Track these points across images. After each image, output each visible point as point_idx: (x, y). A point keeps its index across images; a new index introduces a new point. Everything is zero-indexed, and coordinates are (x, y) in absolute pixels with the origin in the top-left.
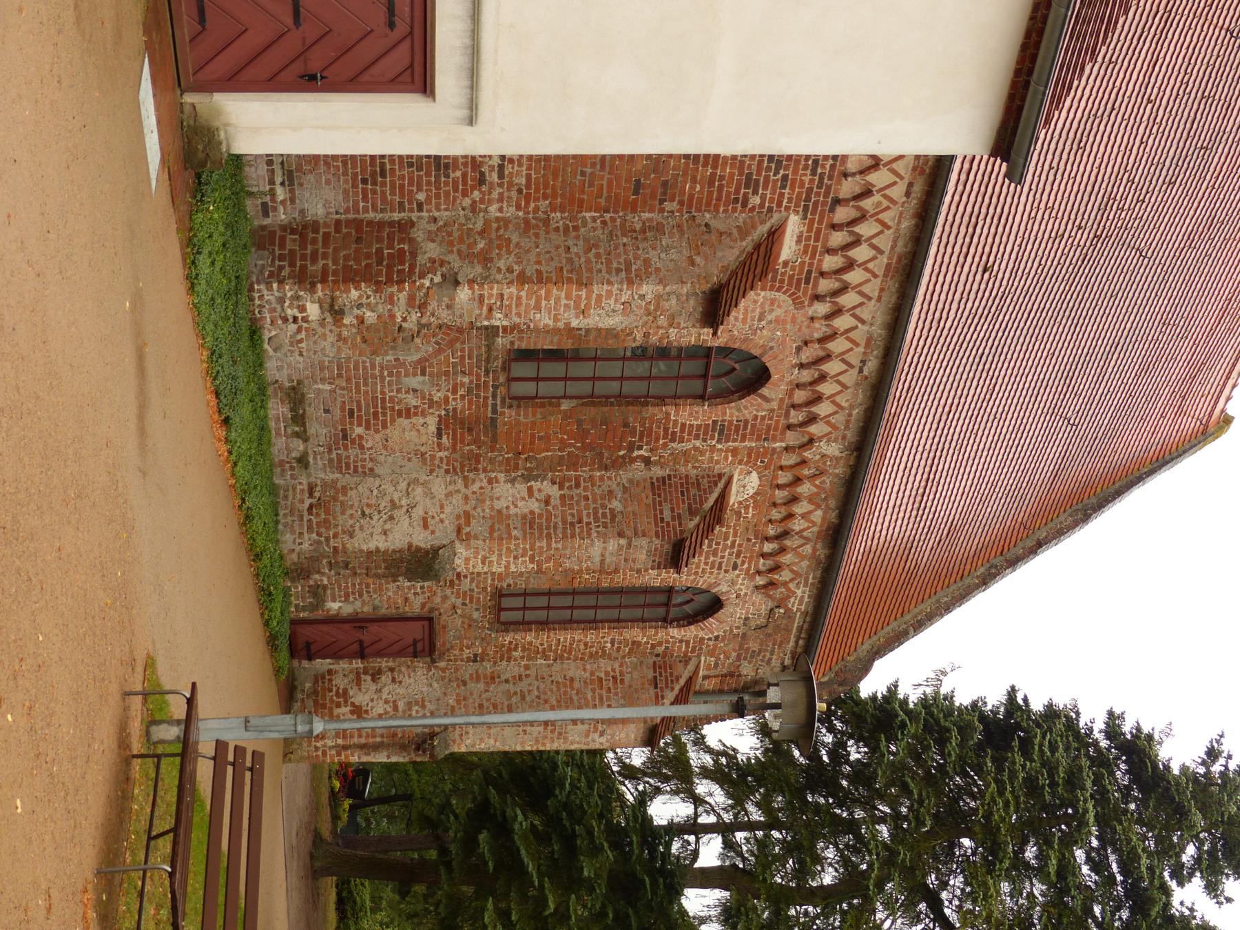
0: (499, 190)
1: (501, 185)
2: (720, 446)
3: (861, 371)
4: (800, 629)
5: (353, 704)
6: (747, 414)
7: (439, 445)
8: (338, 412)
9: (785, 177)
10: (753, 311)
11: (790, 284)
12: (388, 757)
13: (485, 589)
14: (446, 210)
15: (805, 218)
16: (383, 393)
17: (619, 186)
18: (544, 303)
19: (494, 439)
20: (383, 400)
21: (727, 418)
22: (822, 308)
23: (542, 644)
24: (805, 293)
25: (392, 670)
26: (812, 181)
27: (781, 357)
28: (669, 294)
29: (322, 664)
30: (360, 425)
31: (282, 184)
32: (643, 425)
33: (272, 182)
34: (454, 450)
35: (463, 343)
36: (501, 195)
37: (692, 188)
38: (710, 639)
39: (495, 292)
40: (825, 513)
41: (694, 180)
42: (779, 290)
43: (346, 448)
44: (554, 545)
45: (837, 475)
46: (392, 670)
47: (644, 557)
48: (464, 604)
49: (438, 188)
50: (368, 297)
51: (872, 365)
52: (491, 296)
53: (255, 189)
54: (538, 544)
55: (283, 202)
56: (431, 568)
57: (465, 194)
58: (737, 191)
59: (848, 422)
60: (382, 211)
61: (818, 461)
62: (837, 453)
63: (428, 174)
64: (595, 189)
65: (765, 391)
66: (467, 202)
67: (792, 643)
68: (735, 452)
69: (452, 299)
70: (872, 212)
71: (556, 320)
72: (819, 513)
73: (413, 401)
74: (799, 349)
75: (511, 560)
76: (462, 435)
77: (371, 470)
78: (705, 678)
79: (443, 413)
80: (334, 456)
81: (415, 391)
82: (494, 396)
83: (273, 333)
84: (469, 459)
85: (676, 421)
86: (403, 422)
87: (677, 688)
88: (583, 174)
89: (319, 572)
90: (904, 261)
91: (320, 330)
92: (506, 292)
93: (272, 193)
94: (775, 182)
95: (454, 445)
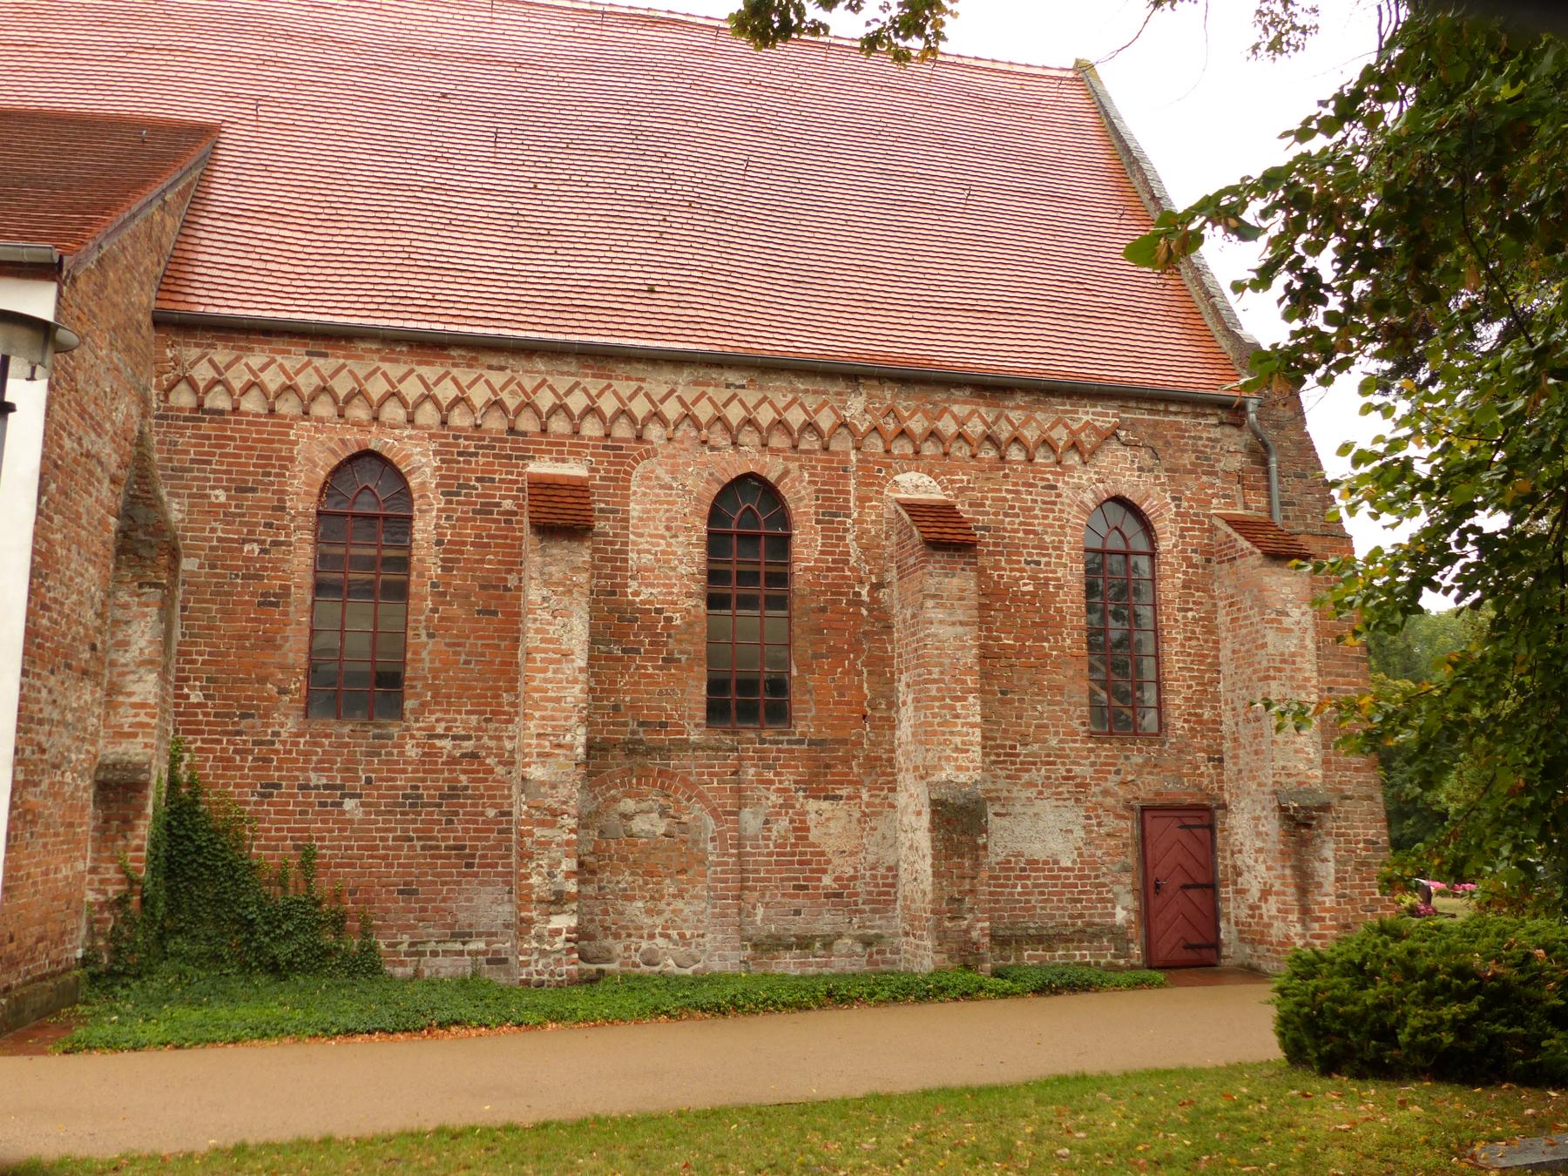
0: (485, 740)
1: (479, 738)
2: (855, 515)
3: (743, 387)
4: (1151, 412)
5: (1260, 900)
6: (805, 490)
7: (849, 798)
8: (799, 902)
9: (478, 480)
10: (657, 495)
11: (622, 464)
12: (1325, 860)
13: (1091, 750)
14: (510, 789)
15: (533, 458)
16: (770, 854)
17: (483, 629)
18: (550, 694)
19: (844, 742)
20: (779, 854)
21: (812, 510)
22: (655, 432)
23: (1190, 687)
24: (634, 449)
25: (1233, 853)
26: (484, 455)
27: (724, 464)
28: (542, 574)
29: (1227, 932)
30: (820, 879)
31: (464, 943)
32: (824, 593)
33: (461, 953)
34: (861, 783)
35: (690, 774)
36: (491, 738)
37: (490, 562)
38: (1178, 506)
39: (534, 742)
40: (956, 402)
41: (482, 561)
42: (630, 474)
43: (857, 895)
44: (935, 676)
45: (895, 396)
46: (1233, 853)
47: (955, 581)
48: (1118, 772)
49: (482, 796)
50: (539, 866)
51: (732, 377)
52: (538, 746)
53: (469, 970)
54: (934, 693)
55: (488, 944)
56: (962, 809)
57: (491, 771)
58: (497, 521)
59: (815, 392)
60: (508, 849)
61: (874, 417)
62: (862, 399)
63: (463, 806)
64: (487, 651)
65: (772, 477)
66: (500, 770)
67: (1179, 418)
68: (862, 500)
69: (543, 783)
70: (523, 397)
71: (576, 681)
72: (956, 408)
73: (782, 824)
74: (712, 448)
75: (959, 721)
76: (833, 775)
77: (889, 869)
78: (1246, 507)
79: (801, 793)
80: (867, 908)
81: (767, 822)
82: (776, 742)
83: (671, 962)
84: (874, 767)
85: (816, 561)
86: (813, 835)
87: (1235, 535)
88: (467, 662)
89: (967, 931)
90: (591, 362)
91: (667, 915)
92: (533, 730)
93: (478, 953)
94: (484, 488)
95: (850, 782)
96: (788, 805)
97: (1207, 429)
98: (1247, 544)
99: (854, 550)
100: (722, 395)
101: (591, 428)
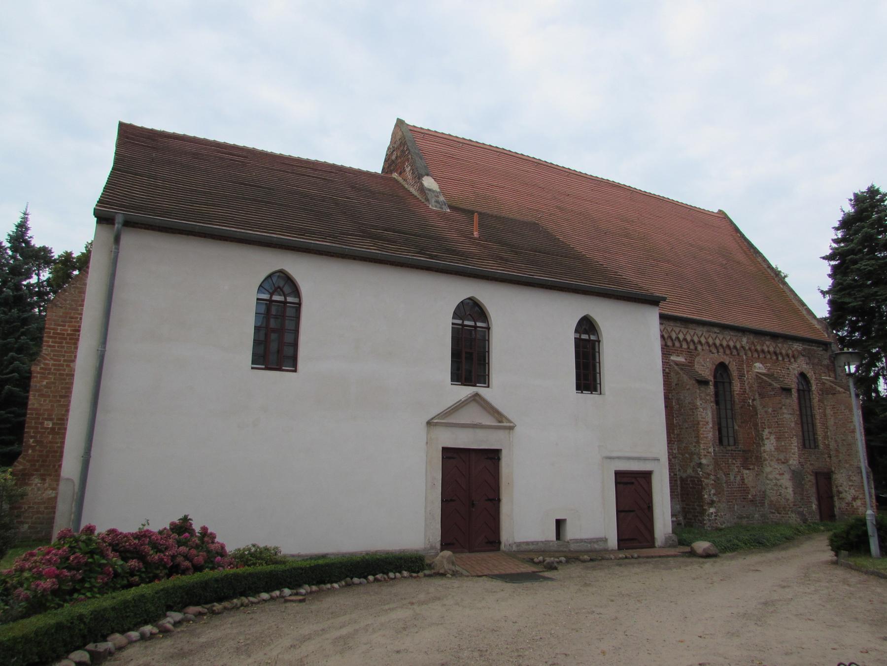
51: (716, 330)
65: (727, 363)
68: (748, 372)
73: (738, 478)
86: (746, 481)
96: (739, 472)
97: (819, 351)
98: (841, 390)
99: (747, 388)
100: (714, 336)
101: (685, 346)
